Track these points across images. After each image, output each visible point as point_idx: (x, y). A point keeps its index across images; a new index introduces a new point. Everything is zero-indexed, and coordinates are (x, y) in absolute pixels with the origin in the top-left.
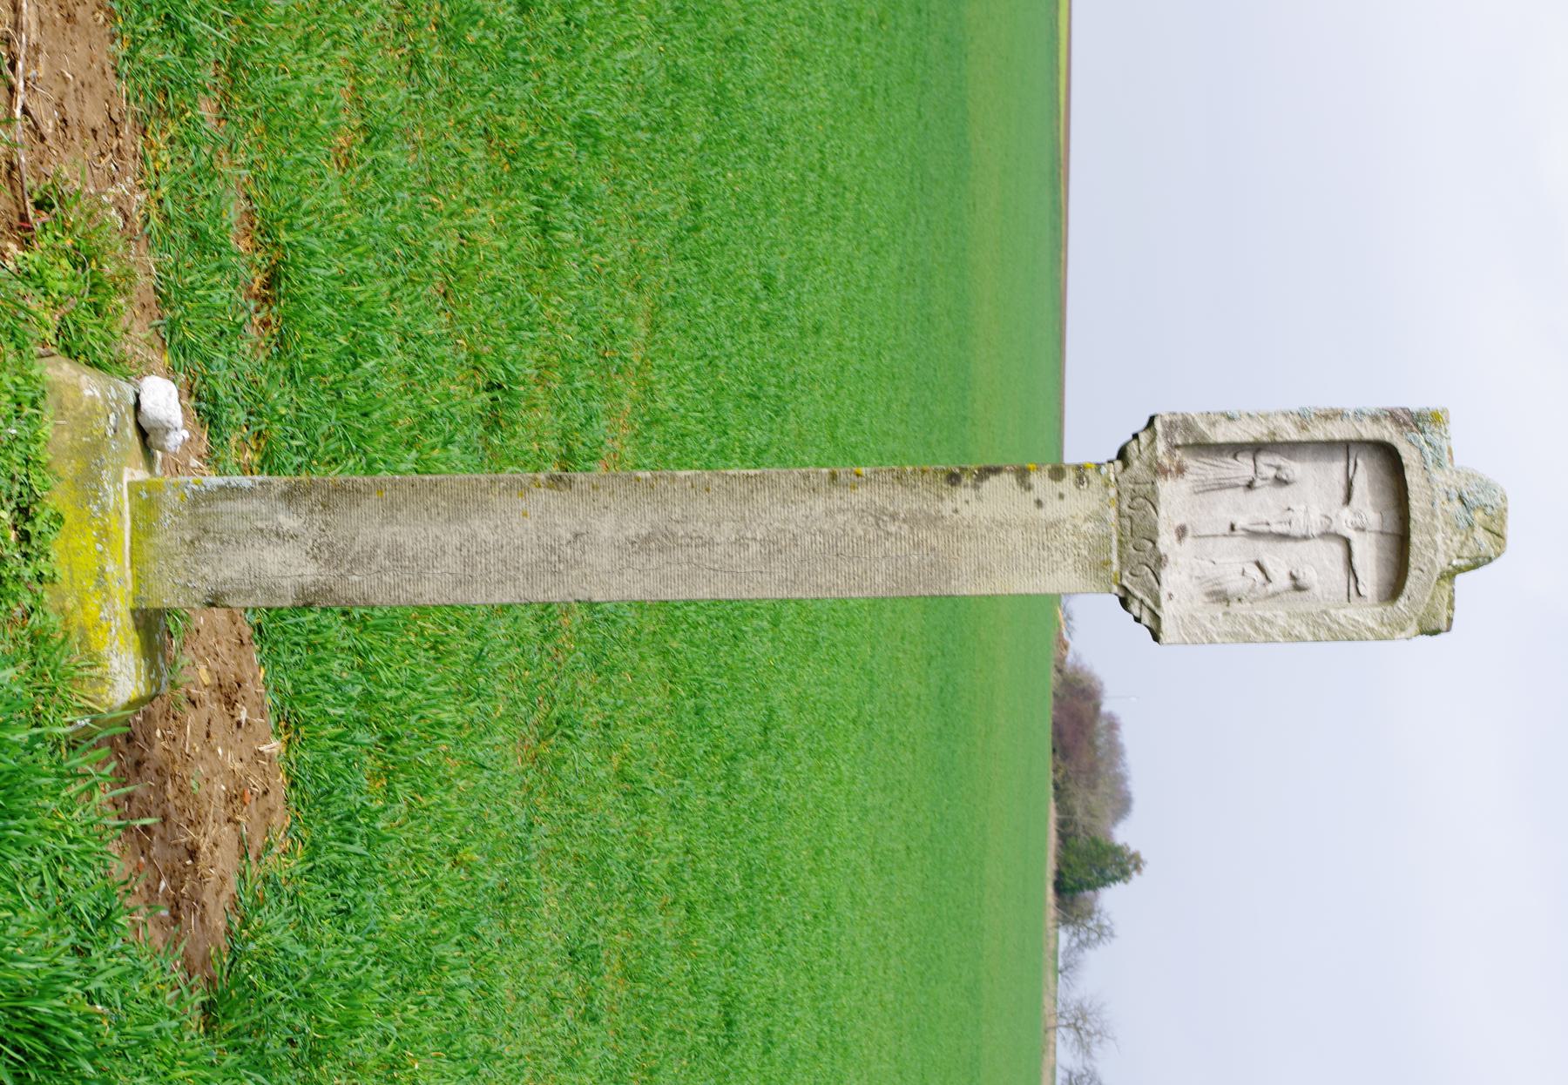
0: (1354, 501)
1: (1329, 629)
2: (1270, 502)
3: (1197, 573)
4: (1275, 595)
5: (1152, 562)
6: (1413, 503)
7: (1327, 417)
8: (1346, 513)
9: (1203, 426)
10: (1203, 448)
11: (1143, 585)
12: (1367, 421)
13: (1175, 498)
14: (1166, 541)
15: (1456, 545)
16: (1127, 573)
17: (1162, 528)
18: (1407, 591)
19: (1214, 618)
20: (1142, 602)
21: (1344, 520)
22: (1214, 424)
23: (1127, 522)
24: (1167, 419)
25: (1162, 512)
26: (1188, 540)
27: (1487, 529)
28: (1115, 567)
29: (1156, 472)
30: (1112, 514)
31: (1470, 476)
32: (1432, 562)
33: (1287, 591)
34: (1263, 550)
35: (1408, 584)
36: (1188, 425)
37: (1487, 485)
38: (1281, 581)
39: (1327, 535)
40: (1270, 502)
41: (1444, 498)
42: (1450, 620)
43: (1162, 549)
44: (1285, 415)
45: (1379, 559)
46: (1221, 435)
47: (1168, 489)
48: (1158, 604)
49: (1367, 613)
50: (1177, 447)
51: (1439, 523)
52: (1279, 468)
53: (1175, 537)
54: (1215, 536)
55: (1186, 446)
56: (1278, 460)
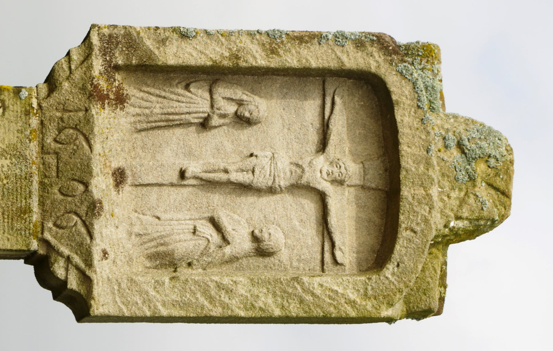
0: (330, 148)
1: (301, 301)
2: (229, 147)
3: (137, 229)
4: (233, 259)
5: (83, 210)
6: (404, 148)
7: (303, 39)
8: (321, 161)
9: (149, 43)
10: (149, 71)
11: (71, 238)
12: (349, 46)
13: (112, 133)
14: (101, 184)
15: (454, 203)
16: (50, 225)
17: (96, 168)
18: (396, 256)
19: (159, 283)
20: (68, 259)
21: (319, 170)
22: (163, 42)
23: (51, 160)
24: (106, 31)
25: (97, 147)
26: (127, 188)
27: (490, 185)
28: (35, 217)
29: (90, 96)
30: (33, 149)
31: (468, 122)
32: (426, 221)
33: (247, 256)
34: (219, 203)
35: (397, 247)
36: (128, 39)
37: (490, 131)
38: (241, 243)
39: (299, 187)
40: (229, 147)
41: (440, 145)
42: (442, 300)
43: (96, 194)
44: (251, 34)
45: (358, 220)
46: (172, 55)
47: (103, 117)
48: (89, 263)
49: (345, 286)
50: (117, 68)
51: (435, 174)
52: (240, 103)
53: (111, 181)
54: (161, 185)
55: (128, 69)
56: (239, 94)
